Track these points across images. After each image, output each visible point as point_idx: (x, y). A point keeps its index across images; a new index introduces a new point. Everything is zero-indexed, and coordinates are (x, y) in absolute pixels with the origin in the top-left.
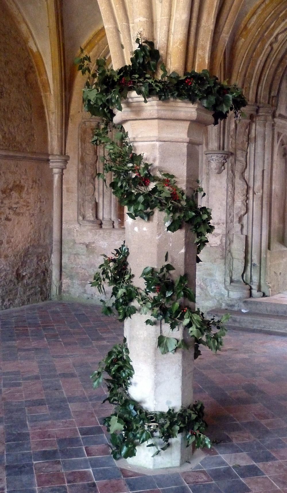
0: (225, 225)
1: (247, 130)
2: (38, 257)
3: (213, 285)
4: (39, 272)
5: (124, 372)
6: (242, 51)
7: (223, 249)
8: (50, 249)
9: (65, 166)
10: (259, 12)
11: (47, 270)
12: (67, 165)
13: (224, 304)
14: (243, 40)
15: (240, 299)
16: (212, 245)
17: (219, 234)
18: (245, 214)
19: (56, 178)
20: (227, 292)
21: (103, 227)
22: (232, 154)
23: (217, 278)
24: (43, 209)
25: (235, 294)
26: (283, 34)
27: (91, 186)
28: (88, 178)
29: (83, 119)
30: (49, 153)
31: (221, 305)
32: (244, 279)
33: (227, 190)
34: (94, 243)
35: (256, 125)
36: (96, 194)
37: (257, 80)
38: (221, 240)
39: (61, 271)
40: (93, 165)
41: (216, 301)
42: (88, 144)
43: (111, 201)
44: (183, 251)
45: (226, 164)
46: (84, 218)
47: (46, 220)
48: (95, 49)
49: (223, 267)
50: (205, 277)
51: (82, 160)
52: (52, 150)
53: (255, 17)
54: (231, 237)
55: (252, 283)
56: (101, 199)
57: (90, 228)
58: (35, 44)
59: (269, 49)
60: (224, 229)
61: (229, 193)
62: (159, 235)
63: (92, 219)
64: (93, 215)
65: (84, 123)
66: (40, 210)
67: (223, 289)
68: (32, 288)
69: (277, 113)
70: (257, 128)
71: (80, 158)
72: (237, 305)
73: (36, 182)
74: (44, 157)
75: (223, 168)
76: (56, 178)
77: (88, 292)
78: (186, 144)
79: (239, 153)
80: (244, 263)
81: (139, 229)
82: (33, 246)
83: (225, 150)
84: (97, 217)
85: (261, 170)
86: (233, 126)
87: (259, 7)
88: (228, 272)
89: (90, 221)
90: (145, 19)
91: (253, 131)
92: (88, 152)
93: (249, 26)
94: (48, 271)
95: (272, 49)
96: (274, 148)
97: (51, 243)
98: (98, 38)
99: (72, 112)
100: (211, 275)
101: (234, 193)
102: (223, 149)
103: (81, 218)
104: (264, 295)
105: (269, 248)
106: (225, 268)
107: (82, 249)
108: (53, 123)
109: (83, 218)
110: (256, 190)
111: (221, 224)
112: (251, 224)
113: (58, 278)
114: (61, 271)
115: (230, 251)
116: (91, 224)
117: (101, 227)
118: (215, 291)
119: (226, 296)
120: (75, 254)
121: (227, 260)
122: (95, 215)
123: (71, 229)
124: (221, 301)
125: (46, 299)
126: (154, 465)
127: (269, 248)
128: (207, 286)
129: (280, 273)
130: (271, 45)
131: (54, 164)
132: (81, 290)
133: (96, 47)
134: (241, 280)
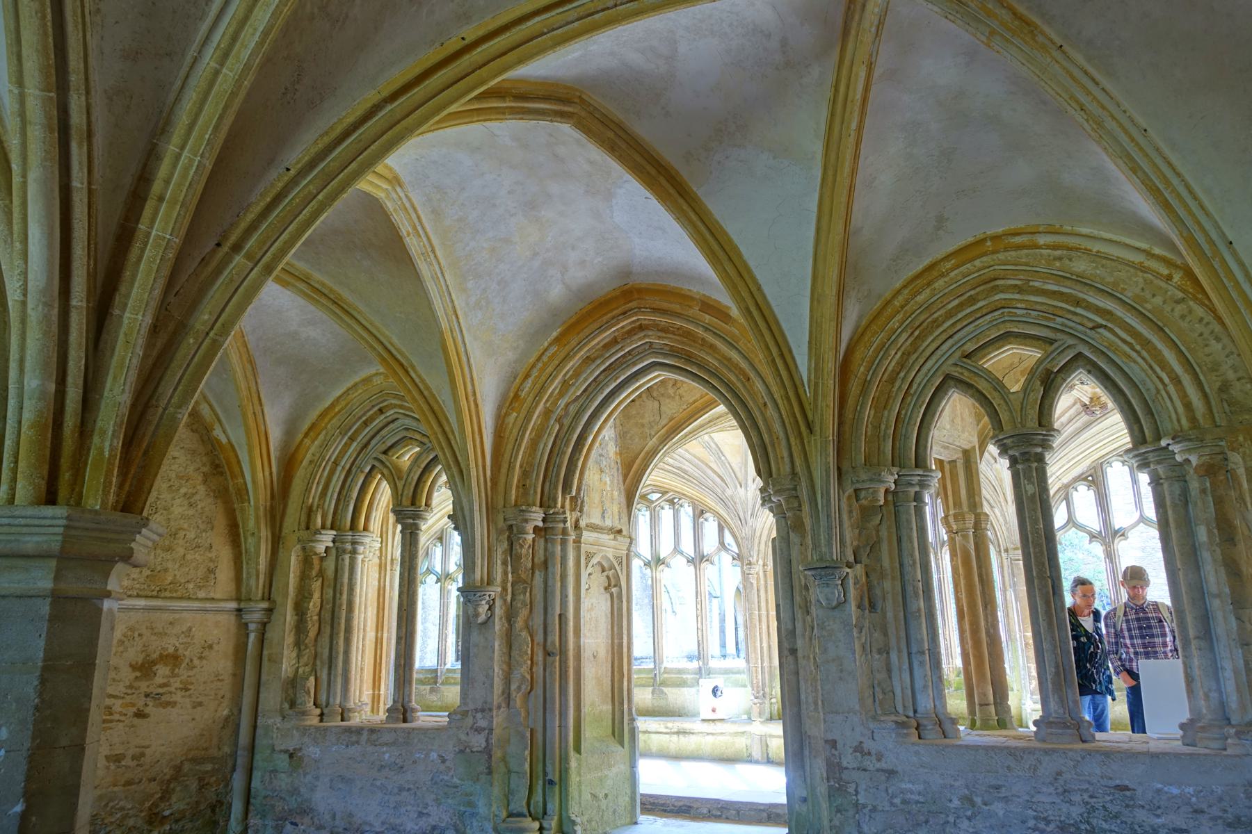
2: (200, 780)
3: (475, 824)
5: (1069, 816)
10: (535, 373)
12: (273, 618)
16: (475, 750)
17: (484, 729)
23: (481, 811)
26: (576, 404)
32: (532, 809)
48: (321, 437)
50: (462, 808)
53: (530, 381)
58: (224, 432)
69: (582, 523)
78: (49, 600)
87: (533, 366)
93: (523, 395)
100: (471, 804)
107: (282, 761)
114: (247, 803)
120: (272, 772)
123: (268, 726)
129: (606, 796)
133: (324, 432)
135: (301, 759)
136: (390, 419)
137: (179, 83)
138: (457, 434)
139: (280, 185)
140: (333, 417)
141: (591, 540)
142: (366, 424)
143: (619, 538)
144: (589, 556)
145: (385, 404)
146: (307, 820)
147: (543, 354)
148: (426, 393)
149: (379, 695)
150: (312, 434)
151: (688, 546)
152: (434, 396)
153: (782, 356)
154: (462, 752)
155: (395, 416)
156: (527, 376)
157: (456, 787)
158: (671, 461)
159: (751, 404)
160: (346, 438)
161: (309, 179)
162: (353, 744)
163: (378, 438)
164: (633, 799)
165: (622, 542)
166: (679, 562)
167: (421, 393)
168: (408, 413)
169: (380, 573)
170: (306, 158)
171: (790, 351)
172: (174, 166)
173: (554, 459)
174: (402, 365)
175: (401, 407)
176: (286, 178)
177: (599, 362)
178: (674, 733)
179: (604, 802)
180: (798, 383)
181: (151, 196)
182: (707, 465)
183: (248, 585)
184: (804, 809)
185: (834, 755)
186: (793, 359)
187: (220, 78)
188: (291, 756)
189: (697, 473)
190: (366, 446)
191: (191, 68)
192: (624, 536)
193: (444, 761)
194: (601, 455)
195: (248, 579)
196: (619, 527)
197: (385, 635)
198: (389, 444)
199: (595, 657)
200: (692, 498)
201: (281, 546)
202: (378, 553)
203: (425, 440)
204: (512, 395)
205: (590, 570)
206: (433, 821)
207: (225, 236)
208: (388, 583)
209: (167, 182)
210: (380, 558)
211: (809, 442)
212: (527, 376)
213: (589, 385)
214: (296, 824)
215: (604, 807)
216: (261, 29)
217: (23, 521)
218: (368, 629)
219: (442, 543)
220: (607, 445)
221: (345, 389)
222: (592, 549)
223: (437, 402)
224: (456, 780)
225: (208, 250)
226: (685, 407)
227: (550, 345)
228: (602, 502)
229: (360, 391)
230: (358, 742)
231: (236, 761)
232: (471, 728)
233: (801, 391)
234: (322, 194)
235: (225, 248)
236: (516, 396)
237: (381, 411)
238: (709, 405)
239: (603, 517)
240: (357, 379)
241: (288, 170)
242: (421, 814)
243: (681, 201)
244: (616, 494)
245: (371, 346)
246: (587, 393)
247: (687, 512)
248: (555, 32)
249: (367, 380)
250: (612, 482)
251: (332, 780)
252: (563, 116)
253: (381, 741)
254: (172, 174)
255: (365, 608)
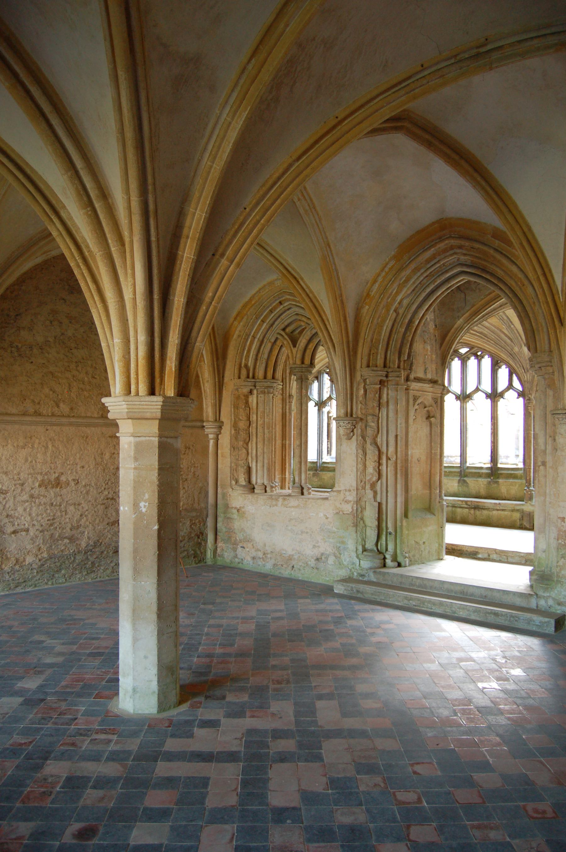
0: (355, 492)
1: (377, 395)
2: (191, 520)
3: (346, 553)
4: (193, 535)
6: (367, 318)
7: (354, 515)
8: (205, 513)
9: (220, 432)
10: (380, 279)
11: (202, 534)
12: (222, 431)
13: (355, 574)
14: (367, 307)
15: (371, 568)
16: (345, 513)
17: (351, 501)
18: (379, 480)
19: (212, 442)
20: (358, 561)
21: (256, 491)
22: (361, 419)
24: (197, 474)
25: (366, 564)
27: (244, 451)
28: (241, 443)
29: (235, 386)
30: (205, 419)
31: (353, 574)
32: (379, 548)
33: (357, 456)
34: (243, 507)
35: (388, 389)
36: (250, 458)
37: (385, 346)
38: (352, 508)
39: (216, 534)
40: (246, 430)
41: (349, 571)
42: (241, 410)
43: (264, 466)
44: (156, 527)
45: (355, 430)
46: (237, 482)
47: (200, 485)
48: (245, 319)
49: (355, 535)
50: (338, 545)
51: (235, 426)
52: (208, 416)
53: (377, 285)
54: (363, 503)
55: (387, 552)
56: (254, 464)
57: (241, 492)
59: (395, 314)
60: (355, 496)
61: (360, 459)
62: (135, 514)
63: (244, 483)
64: (245, 479)
65: (237, 390)
66: (194, 475)
67: (355, 558)
68: (184, 551)
69: (412, 377)
70: (388, 393)
71: (233, 423)
72: (367, 575)
73: (189, 448)
74: (199, 424)
75: (352, 434)
76: (212, 442)
77: (239, 556)
79: (370, 418)
80: (376, 532)
81: (123, 508)
82: (186, 509)
83: (354, 416)
84: (250, 481)
85: (394, 434)
86: (362, 392)
87: (379, 275)
88: (360, 540)
89: (241, 486)
90: (120, 340)
91: (385, 396)
92: (241, 418)
93: (372, 294)
94: (203, 535)
95: (398, 314)
96: (409, 412)
97: (206, 508)
98: (247, 309)
99: (226, 379)
100: (343, 542)
101: (366, 460)
102: (351, 415)
103: (234, 482)
104: (399, 565)
105: (406, 516)
106: (357, 536)
108: (208, 390)
109: (236, 483)
110: (389, 455)
111: (352, 491)
112: (385, 491)
113: (213, 542)
114: (216, 534)
115: (362, 519)
116: (242, 489)
117: (254, 492)
118: (348, 560)
119: (358, 565)
121: (358, 528)
122: (247, 480)
124: (353, 570)
125: (200, 561)
126: (134, 710)
127: (406, 516)
128: (340, 554)
129: (424, 543)
130: (395, 311)
131: (209, 430)
132: (232, 554)
133: (246, 317)
134: (375, 549)
135: (244, 513)
136: (287, 308)
137: (192, 174)
138: (330, 321)
139: (242, 218)
140: (251, 307)
141: (417, 388)
142: (271, 311)
143: (436, 386)
144: (415, 399)
145: (283, 298)
146: (250, 545)
147: (385, 267)
148: (311, 295)
149: (285, 478)
150: (238, 318)
151: (487, 386)
152: (315, 297)
153: (545, 275)
154: (337, 513)
155: (289, 307)
156: (375, 281)
157: (335, 533)
158: (472, 332)
159: (525, 302)
160: (260, 320)
161: (255, 212)
162: (273, 506)
163: (279, 320)
164: (440, 545)
165: (438, 389)
166: (479, 397)
167: (308, 295)
168: (298, 304)
169: (283, 404)
170: (254, 201)
171: (550, 271)
172: (193, 219)
173: (393, 336)
174: (295, 278)
175: (294, 300)
176: (244, 214)
177: (422, 271)
178: (472, 508)
179: (423, 546)
180: (554, 292)
181: (183, 236)
182: (501, 330)
183: (207, 412)
184: (544, 555)
185: (563, 526)
186: (552, 276)
187: (213, 170)
188: (238, 511)
189: (493, 336)
190: (272, 325)
191: (198, 166)
192: (440, 385)
193: (327, 518)
194: (424, 331)
195: (207, 408)
196: (436, 379)
197: (287, 442)
198: (286, 323)
199: (419, 461)
200: (490, 352)
201: (224, 388)
202: (281, 392)
203: (309, 322)
204: (365, 294)
205: (416, 407)
206: (322, 550)
207: (216, 250)
208: (287, 411)
209: (190, 228)
210: (282, 395)
211: (560, 332)
212: (375, 281)
213: (416, 287)
214: (244, 548)
215: (423, 549)
216: (232, 142)
217: (144, 403)
218: (277, 438)
219: (318, 380)
220: (428, 324)
221: (257, 289)
222: (418, 394)
223: (318, 301)
224: (334, 529)
225: (208, 258)
226: (482, 297)
227: (390, 260)
228: (425, 363)
229: (267, 290)
230: (276, 505)
231: (208, 511)
232: (343, 500)
233: (556, 297)
234: (263, 220)
235: (217, 256)
236: (368, 295)
237: (281, 303)
238: (497, 298)
239: (425, 373)
240: (265, 283)
241: (245, 209)
242: (314, 547)
243: (476, 175)
244: (434, 356)
245: (276, 267)
246: (415, 292)
247: (487, 362)
248: (391, 104)
249: (271, 283)
250: (432, 349)
251: (263, 525)
252: (396, 129)
253: (290, 505)
254: (192, 224)
255: (275, 426)
